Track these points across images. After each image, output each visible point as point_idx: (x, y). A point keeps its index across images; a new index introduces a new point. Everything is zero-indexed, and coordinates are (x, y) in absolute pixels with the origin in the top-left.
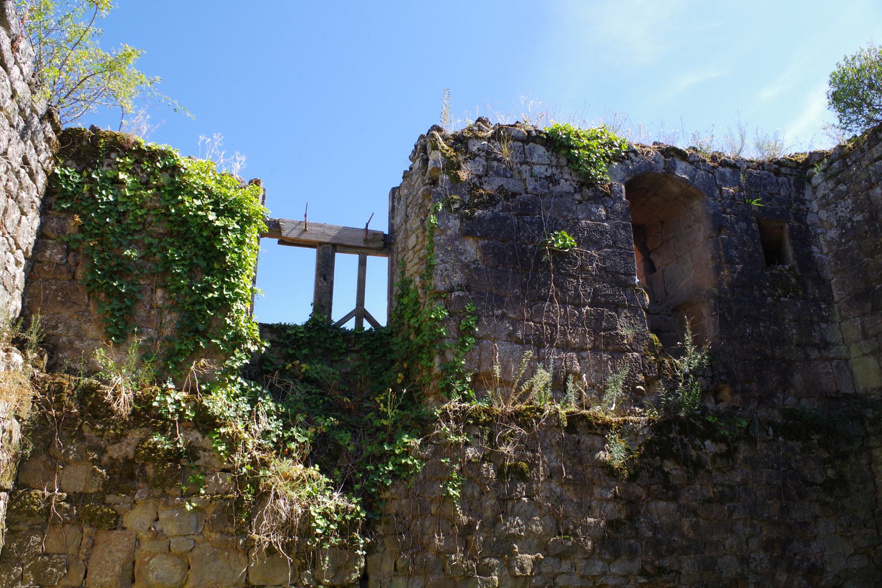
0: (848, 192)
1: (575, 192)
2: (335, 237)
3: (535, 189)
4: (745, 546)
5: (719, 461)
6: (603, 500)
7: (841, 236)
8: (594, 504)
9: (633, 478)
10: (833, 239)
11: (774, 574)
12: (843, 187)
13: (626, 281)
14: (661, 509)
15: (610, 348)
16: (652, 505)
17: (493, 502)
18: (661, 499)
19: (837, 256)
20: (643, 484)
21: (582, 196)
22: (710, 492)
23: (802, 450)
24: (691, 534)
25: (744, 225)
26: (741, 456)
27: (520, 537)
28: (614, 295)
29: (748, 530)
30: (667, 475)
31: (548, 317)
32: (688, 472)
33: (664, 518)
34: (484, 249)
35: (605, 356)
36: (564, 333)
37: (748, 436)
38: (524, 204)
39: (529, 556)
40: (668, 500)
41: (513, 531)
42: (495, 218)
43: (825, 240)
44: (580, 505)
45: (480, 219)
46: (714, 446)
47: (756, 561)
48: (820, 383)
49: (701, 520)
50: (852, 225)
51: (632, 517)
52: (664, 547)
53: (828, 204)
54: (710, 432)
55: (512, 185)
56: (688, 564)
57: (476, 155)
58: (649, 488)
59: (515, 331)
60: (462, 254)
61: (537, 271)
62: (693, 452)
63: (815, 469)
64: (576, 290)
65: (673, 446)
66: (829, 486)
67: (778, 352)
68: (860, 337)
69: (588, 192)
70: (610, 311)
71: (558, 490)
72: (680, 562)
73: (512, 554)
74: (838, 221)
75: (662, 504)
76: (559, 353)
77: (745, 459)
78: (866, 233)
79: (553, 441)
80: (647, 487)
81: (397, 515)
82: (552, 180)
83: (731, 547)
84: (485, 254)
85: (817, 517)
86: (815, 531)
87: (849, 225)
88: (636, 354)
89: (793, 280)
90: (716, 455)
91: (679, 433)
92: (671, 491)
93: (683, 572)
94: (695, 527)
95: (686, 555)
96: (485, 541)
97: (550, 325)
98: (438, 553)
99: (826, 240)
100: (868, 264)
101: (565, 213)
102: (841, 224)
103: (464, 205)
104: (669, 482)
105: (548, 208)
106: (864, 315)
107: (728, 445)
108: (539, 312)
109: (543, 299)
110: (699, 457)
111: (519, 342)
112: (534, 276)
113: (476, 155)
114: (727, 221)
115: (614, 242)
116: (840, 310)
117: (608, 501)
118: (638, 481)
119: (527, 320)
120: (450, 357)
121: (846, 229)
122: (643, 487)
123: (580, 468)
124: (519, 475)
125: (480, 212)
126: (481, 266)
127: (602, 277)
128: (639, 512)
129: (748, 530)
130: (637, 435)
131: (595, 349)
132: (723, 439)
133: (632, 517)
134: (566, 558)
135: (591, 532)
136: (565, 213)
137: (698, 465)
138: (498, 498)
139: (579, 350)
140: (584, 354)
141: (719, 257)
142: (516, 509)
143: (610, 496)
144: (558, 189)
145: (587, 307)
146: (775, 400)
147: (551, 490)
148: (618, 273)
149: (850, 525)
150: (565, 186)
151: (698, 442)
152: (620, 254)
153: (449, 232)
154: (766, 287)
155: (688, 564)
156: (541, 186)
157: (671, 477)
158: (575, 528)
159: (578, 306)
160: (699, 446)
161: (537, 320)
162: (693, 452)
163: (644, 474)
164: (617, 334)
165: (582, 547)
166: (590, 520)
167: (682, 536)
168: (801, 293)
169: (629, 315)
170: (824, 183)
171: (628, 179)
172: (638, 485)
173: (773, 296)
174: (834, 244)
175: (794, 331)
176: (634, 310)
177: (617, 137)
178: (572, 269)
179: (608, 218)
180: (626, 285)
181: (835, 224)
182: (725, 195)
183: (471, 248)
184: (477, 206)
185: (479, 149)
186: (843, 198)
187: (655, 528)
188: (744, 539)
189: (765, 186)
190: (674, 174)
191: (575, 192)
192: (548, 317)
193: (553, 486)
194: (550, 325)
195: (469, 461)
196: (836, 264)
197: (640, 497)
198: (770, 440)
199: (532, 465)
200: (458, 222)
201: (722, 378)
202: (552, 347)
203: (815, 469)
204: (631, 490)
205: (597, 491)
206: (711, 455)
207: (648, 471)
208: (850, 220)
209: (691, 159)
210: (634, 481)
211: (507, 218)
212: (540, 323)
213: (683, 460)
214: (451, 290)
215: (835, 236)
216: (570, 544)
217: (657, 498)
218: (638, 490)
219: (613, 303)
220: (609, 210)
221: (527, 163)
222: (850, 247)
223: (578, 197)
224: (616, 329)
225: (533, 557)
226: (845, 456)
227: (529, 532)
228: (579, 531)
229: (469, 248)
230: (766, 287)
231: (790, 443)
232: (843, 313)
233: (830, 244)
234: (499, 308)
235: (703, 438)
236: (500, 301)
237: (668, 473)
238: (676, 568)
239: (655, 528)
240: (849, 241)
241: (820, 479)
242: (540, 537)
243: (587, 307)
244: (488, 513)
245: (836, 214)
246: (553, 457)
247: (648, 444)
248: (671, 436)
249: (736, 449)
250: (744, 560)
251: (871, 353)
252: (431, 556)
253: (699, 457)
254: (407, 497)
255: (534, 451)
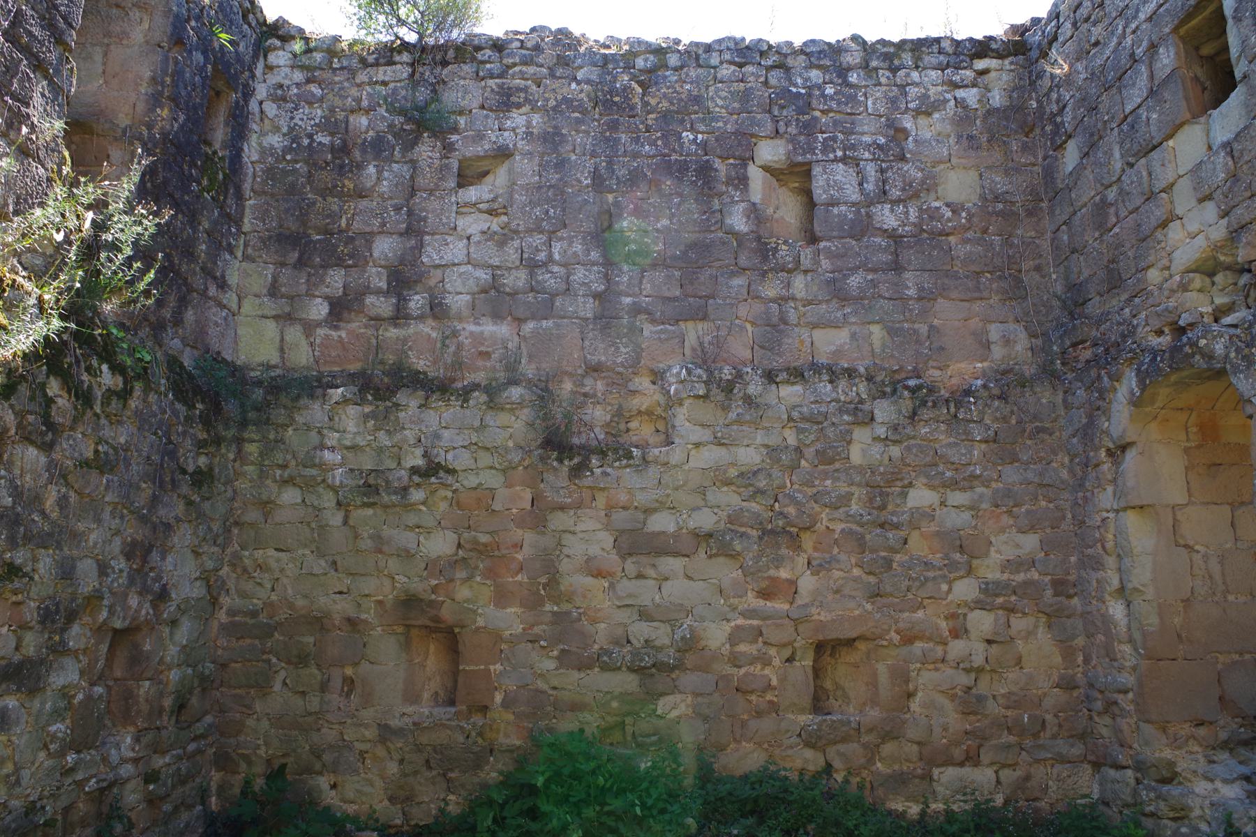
0: (321, 100)
7: (288, 150)
10: (272, 147)
11: (127, 595)
12: (315, 89)
13: (62, 33)
16: (18, 449)
18: (32, 443)
19: (270, 172)
20: (17, 408)
28: (41, 43)
32: (76, 408)
43: (260, 144)
47: (114, 572)
49: (72, 494)
50: (310, 144)
53: (284, 99)
56: (45, 564)
58: (23, 417)
62: (85, 377)
67: (184, 268)
68: (265, 291)
72: (35, 560)
74: (291, 129)
75: (32, 452)
78: (327, 164)
80: (20, 415)
87: (306, 142)
89: (221, 176)
93: (36, 577)
94: (63, 502)
95: (45, 548)
99: (264, 142)
100: (314, 203)
102: (293, 134)
106: (283, 265)
110: (90, 387)
116: (246, 246)
118: (13, 401)
121: (299, 145)
141: (163, 83)
151: (95, 363)
155: (45, 564)
157: (54, 407)
162: (85, 377)
167: (43, 513)
169: (46, 92)
170: (288, 70)
174: (272, 155)
181: (285, 130)
186: (310, 104)
196: (264, 182)
206: (104, 388)
208: (310, 136)
215: (276, 145)
217: (28, 439)
222: (295, 170)
226: (218, 441)
232: (250, 250)
233: (264, 152)
238: (28, 569)
240: (296, 162)
245: (292, 118)
250: (103, 569)
251: (274, 317)
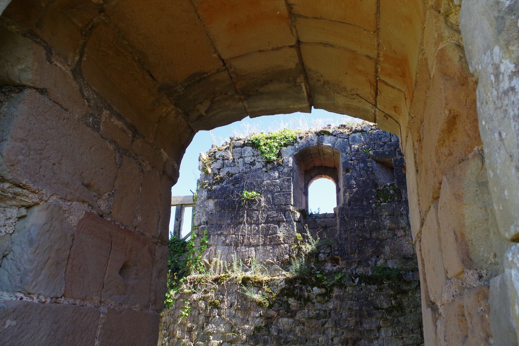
1: (263, 167)
2: (181, 201)
3: (243, 170)
4: (330, 342)
5: (318, 298)
6: (255, 317)
8: (249, 319)
9: (271, 307)
14: (284, 322)
15: (272, 243)
17: (203, 317)
21: (267, 169)
22: (312, 313)
23: (376, 290)
24: (300, 335)
25: (362, 165)
26: (334, 295)
27: (213, 333)
29: (333, 333)
30: (289, 305)
31: (242, 232)
33: (286, 326)
34: (216, 204)
35: (269, 248)
36: (249, 239)
37: (340, 285)
38: (236, 179)
39: (216, 341)
40: (288, 317)
41: (210, 330)
42: (222, 188)
44: (242, 319)
45: (215, 190)
46: (319, 289)
48: (402, 250)
51: (268, 326)
52: (283, 340)
54: (318, 283)
55: (232, 170)
57: (218, 159)
58: (279, 312)
59: (226, 240)
60: (206, 208)
61: (239, 210)
62: (306, 294)
63: (383, 301)
64: (258, 216)
65: (295, 290)
66: (389, 311)
69: (269, 166)
70: (275, 224)
71: (234, 312)
73: (209, 341)
75: (285, 320)
76: (246, 248)
77: (336, 297)
79: (234, 290)
80: (278, 311)
81: (164, 323)
82: (253, 164)
83: (322, 341)
84: (216, 206)
85: (381, 327)
86: (377, 334)
88: (287, 245)
90: (319, 295)
91: (300, 284)
92: (291, 313)
94: (302, 331)
96: (198, 334)
97: (242, 235)
98: (178, 339)
101: (257, 179)
103: (210, 185)
104: (290, 309)
105: (248, 178)
107: (326, 289)
108: (238, 230)
109: (241, 223)
111: (227, 245)
112: (237, 213)
113: (218, 159)
114: (351, 165)
115: (281, 189)
117: (257, 318)
118: (273, 308)
119: (232, 234)
120: (196, 255)
122: (276, 311)
123: (245, 302)
124: (215, 306)
125: (215, 186)
126: (214, 212)
127: (272, 208)
128: (272, 323)
129: (333, 333)
130: (277, 286)
131: (264, 245)
132: (323, 286)
133: (268, 326)
134: (234, 343)
135: (246, 332)
136: (257, 179)
137: (308, 300)
138: (205, 316)
139: (256, 246)
140: (258, 248)
142: (213, 321)
143: (257, 315)
144: (255, 167)
145: (263, 225)
146: (370, 262)
147: (230, 312)
148: (281, 205)
149: (402, 332)
150: (258, 165)
151: (309, 288)
152: (283, 195)
153: (202, 198)
154: (372, 199)
156: (246, 168)
157: (291, 306)
158: (239, 330)
159: (258, 225)
160: (310, 290)
161: (237, 234)
162: (306, 294)
163: (276, 305)
164: (277, 236)
165: (241, 339)
166: (247, 326)
168: (396, 199)
171: (295, 153)
172: (273, 310)
173: (376, 203)
175: (388, 222)
176: (289, 222)
177: (288, 134)
178: (254, 207)
179: (279, 177)
180: (285, 211)
182: (352, 150)
183: (211, 204)
184: (214, 184)
185: (219, 156)
187: (279, 331)
188: (330, 338)
189: (380, 139)
190: (322, 145)
191: (263, 167)
192: (242, 232)
193: (231, 311)
194: (242, 235)
195: (194, 300)
197: (274, 316)
198: (355, 286)
199: (222, 301)
200: (206, 193)
201: (335, 253)
202: (242, 245)
203: (383, 301)
204: (269, 312)
205: (252, 313)
207: (278, 303)
209: (334, 134)
210: (271, 308)
211: (227, 187)
212: (238, 235)
213: (299, 298)
214: (200, 225)
216: (235, 337)
217: (282, 317)
218: (272, 313)
219: (277, 220)
220: (281, 173)
221: (241, 157)
223: (264, 169)
224: (276, 233)
225: (218, 342)
227: (218, 331)
228: (240, 331)
229: (210, 204)
230: (372, 199)
231: (369, 287)
234: (219, 230)
235: (313, 286)
236: (220, 227)
237: (290, 304)
239: (279, 331)
241: (385, 306)
242: (222, 333)
243: (263, 225)
244: (201, 323)
246: (233, 297)
247: (282, 290)
248: (296, 285)
249: (332, 291)
252: (176, 340)
253: (309, 296)
254: (168, 315)
255: (223, 295)
